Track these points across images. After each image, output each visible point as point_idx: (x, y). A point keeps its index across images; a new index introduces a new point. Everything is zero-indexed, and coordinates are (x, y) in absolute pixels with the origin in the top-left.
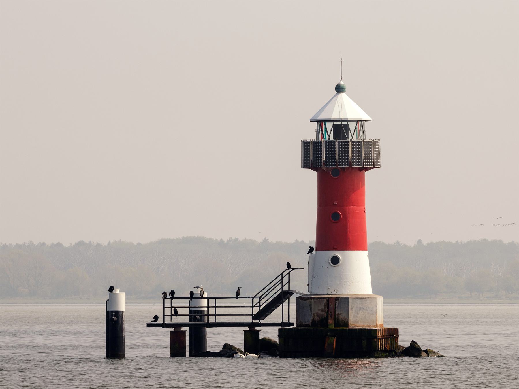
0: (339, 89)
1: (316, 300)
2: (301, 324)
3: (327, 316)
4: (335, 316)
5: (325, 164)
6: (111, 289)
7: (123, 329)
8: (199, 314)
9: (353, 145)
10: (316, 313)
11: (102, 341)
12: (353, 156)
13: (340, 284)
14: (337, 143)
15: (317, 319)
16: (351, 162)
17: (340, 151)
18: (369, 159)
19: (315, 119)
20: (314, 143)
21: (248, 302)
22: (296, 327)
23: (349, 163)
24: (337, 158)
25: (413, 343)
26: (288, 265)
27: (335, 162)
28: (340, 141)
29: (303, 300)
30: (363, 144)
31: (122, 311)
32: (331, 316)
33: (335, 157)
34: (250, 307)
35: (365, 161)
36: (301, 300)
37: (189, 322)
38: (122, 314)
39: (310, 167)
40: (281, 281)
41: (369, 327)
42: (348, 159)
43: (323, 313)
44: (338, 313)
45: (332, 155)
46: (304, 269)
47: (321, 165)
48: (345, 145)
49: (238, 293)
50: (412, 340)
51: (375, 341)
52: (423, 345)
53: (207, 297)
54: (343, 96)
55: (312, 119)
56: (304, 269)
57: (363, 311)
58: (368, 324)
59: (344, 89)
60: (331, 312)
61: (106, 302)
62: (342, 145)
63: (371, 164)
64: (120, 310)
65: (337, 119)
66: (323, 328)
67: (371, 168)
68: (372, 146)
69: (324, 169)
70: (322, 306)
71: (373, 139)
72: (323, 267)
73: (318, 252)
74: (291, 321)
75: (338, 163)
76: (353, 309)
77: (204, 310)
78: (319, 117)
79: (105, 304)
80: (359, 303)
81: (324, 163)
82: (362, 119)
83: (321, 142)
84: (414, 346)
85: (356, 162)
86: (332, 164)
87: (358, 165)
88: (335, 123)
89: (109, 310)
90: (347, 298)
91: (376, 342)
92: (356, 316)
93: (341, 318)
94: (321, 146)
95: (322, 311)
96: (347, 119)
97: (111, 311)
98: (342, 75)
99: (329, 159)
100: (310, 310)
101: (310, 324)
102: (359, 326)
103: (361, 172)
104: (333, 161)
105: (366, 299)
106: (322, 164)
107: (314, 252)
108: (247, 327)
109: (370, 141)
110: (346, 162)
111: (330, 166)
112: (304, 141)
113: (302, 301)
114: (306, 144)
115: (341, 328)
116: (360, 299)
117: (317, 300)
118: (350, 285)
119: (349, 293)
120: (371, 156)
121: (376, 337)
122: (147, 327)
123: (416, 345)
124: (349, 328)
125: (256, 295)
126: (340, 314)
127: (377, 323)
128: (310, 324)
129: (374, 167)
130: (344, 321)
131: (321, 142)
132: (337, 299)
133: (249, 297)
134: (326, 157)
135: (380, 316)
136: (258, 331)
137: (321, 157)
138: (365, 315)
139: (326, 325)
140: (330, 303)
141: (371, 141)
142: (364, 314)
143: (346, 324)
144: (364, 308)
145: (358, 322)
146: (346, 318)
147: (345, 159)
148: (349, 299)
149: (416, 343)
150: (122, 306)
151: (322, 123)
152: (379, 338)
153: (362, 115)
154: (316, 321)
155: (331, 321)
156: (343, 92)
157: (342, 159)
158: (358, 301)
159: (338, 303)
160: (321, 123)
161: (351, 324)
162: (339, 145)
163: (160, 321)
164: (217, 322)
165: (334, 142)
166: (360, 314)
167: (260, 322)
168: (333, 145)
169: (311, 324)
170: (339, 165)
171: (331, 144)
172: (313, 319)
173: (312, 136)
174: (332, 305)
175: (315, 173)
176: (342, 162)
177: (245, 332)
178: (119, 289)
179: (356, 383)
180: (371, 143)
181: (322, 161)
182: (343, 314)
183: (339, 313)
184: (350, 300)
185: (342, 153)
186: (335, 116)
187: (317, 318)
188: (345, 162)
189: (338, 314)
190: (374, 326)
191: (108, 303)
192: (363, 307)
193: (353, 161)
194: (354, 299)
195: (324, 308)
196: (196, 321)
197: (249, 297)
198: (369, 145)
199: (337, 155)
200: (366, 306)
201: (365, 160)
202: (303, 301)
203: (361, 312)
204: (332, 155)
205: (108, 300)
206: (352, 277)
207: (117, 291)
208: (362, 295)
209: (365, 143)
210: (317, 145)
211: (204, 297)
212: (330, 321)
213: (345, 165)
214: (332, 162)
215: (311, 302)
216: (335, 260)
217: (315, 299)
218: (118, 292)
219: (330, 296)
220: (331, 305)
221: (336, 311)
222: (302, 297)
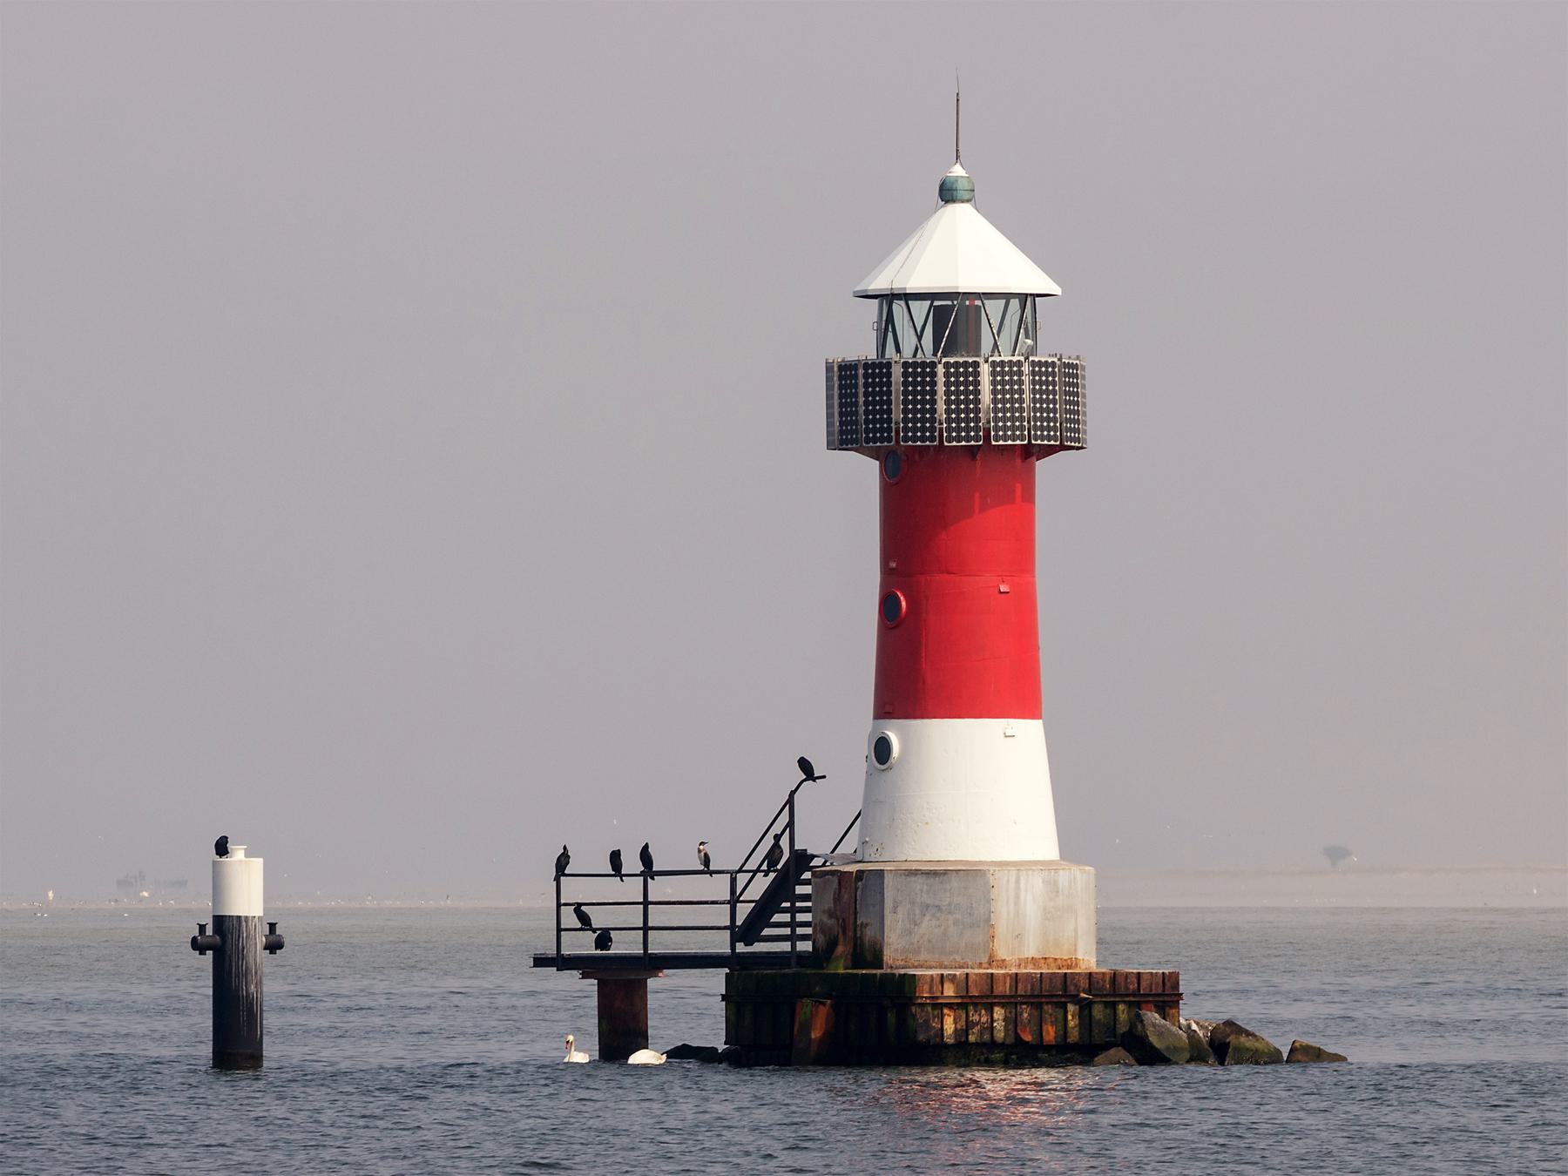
4: (855, 931)
6: (222, 848)
9: (994, 374)
16: (987, 432)
17: (971, 392)
18: (1048, 419)
21: (718, 888)
23: (981, 433)
28: (952, 360)
46: (824, 777)
48: (966, 374)
56: (824, 777)
57: (938, 915)
58: (958, 958)
59: (955, 193)
62: (957, 375)
63: (1055, 435)
64: (232, 914)
71: (1061, 356)
75: (945, 434)
76: (900, 910)
80: (921, 891)
85: (1005, 428)
87: (1014, 438)
88: (937, 303)
92: (910, 933)
93: (867, 938)
98: (960, 145)
102: (921, 963)
104: (928, 425)
105: (945, 877)
110: (972, 429)
111: (928, 443)
116: (924, 876)
118: (915, 832)
119: (913, 856)
125: (743, 865)
126: (867, 924)
129: (1063, 448)
138: (945, 929)
141: (1056, 360)
145: (917, 951)
146: (879, 938)
148: (886, 875)
153: (1025, 276)
158: (918, 884)
161: (894, 959)
162: (947, 375)
165: (933, 365)
166: (923, 925)
168: (971, 374)
173: (863, 348)
176: (958, 429)
180: (1054, 368)
184: (888, 880)
188: (923, 430)
189: (862, 924)
190: (981, 963)
192: (937, 903)
194: (903, 877)
198: (1047, 374)
199: (941, 406)
200: (948, 900)
203: (927, 918)
207: (238, 854)
209: (1034, 367)
210: (878, 370)
221: (858, 916)
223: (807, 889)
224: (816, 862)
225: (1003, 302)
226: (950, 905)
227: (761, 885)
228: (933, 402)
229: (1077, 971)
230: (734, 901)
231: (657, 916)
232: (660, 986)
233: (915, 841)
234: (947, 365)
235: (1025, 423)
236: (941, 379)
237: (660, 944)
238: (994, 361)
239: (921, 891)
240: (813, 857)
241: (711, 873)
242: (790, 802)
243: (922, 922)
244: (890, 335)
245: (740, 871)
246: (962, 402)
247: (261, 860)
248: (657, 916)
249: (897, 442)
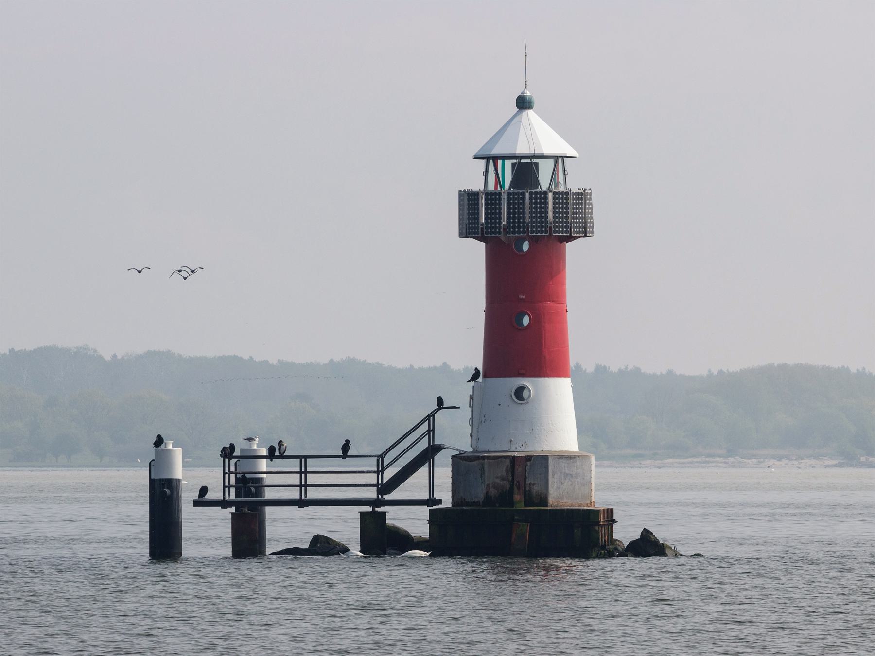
0: (523, 103)
1: (491, 461)
2: (462, 502)
3: (512, 488)
4: (525, 488)
5: (507, 230)
6: (159, 441)
7: (180, 510)
8: (255, 485)
9: (554, 198)
10: (493, 483)
11: (144, 529)
12: (555, 217)
13: (531, 433)
14: (527, 196)
15: (493, 492)
16: (551, 228)
19: (486, 153)
22: (451, 506)
23: (548, 229)
24: (528, 220)
25: (646, 533)
26: (440, 401)
27: (524, 227)
29: (466, 461)
30: (550, 195)
31: (179, 479)
32: (519, 489)
33: (524, 218)
34: (374, 472)
35: (574, 226)
36: (461, 461)
37: (236, 498)
38: (178, 484)
39: (480, 235)
40: (425, 427)
41: (579, 506)
42: (546, 222)
43: (505, 482)
44: (530, 482)
45: (514, 216)
46: (459, 408)
47: (500, 233)
48: (518, 199)
49: (346, 447)
50: (644, 528)
51: (596, 530)
52: (661, 534)
53: (239, 455)
54: (530, 114)
55: (478, 154)
56: (459, 408)
57: (571, 479)
60: (518, 482)
61: (150, 464)
62: (536, 198)
65: (487, 154)
66: (506, 508)
68: (582, 198)
69: (503, 240)
70: (502, 471)
72: (499, 405)
73: (488, 379)
74: (437, 496)
75: (530, 230)
77: (262, 478)
78: (492, 149)
79: (148, 469)
80: (564, 466)
81: (505, 230)
82: (566, 154)
83: (500, 194)
84: (648, 538)
86: (537, 230)
89: (156, 478)
90: (545, 458)
91: (598, 532)
93: (535, 491)
94: (500, 199)
95: (503, 479)
96: (543, 153)
97: (161, 479)
99: (514, 223)
100: (481, 477)
101: (481, 502)
103: (562, 244)
105: (575, 460)
106: (502, 230)
107: (480, 380)
108: (369, 507)
109: (580, 191)
113: (464, 462)
115: (536, 508)
117: (493, 461)
120: (567, 216)
121: (597, 523)
122: (194, 506)
123: (651, 536)
124: (549, 508)
126: (534, 484)
127: (591, 501)
128: (481, 502)
130: (541, 497)
131: (500, 194)
132: (529, 458)
133: (371, 456)
134: (509, 218)
136: (384, 514)
137: (500, 218)
138: (574, 486)
139: (512, 503)
140: (517, 467)
141: (582, 191)
142: (572, 485)
143: (543, 500)
144: (571, 475)
147: (541, 222)
149: (652, 533)
150: (178, 472)
151: (496, 161)
152: (602, 526)
154: (491, 497)
155: (519, 496)
156: (530, 107)
157: (536, 222)
158: (563, 463)
159: (530, 466)
160: (491, 159)
162: (531, 198)
163: (209, 496)
164: (307, 498)
166: (565, 484)
167: (384, 498)
169: (483, 502)
170: (532, 232)
171: (518, 197)
172: (487, 492)
173: (477, 185)
174: (520, 470)
175: (482, 245)
176: (537, 227)
177: (362, 514)
178: (172, 442)
181: (502, 225)
182: (538, 484)
183: (533, 482)
184: (550, 461)
185: (536, 213)
186: (522, 149)
187: (493, 492)
188: (541, 227)
190: (587, 504)
191: (153, 465)
192: (571, 473)
193: (555, 225)
194: (557, 459)
195: (506, 474)
196: (251, 496)
197: (371, 456)
199: (528, 215)
201: (574, 225)
202: (467, 463)
203: (567, 480)
204: (536, 215)
205: (153, 460)
206: (550, 422)
208: (566, 452)
210: (493, 198)
211: (375, 457)
212: (517, 497)
213: (541, 232)
214: (519, 227)
215: (483, 464)
216: (519, 393)
217: (490, 459)
218: (170, 447)
219: (516, 454)
220: (517, 470)
222: (464, 455)
226: (576, 474)
228: (524, 213)
229: (592, 508)
231: (295, 479)
233: (547, 441)
234: (531, 194)
235: (569, 225)
236: (527, 200)
238: (531, 192)
239: (564, 466)
243: (564, 483)
246: (539, 213)
247: (181, 449)
248: (311, 479)
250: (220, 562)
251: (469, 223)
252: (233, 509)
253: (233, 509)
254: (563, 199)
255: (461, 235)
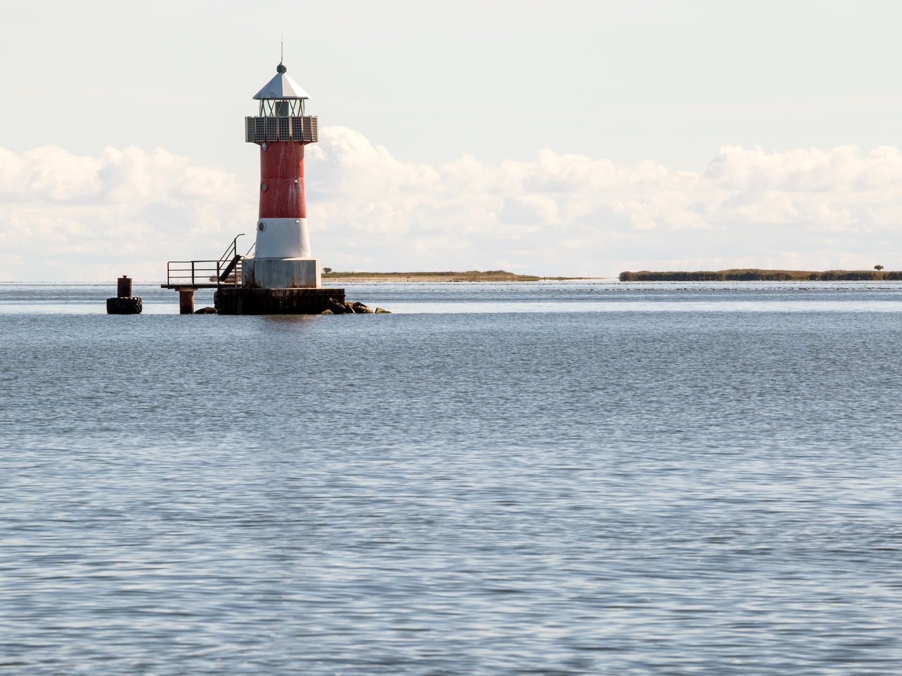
20: (257, 118)
30: (302, 119)
61: (168, 264)
67: (309, 142)
94: (288, 121)
112: (248, 117)
114: (250, 121)
135: (746, 530)
173: (255, 113)
176: (283, 137)
179: (786, 317)
188: (286, 137)
223: (240, 266)
224: (242, 258)
225: (295, 100)
227: (227, 264)
230: (218, 269)
232: (197, 294)
237: (197, 281)
240: (241, 257)
241: (192, 262)
242: (235, 241)
244: (263, 110)
245: (221, 261)
249: (278, 140)
250: (177, 315)
251: (257, 134)
252: (216, 289)
253: (216, 289)
254: (261, 121)
255: (246, 142)
